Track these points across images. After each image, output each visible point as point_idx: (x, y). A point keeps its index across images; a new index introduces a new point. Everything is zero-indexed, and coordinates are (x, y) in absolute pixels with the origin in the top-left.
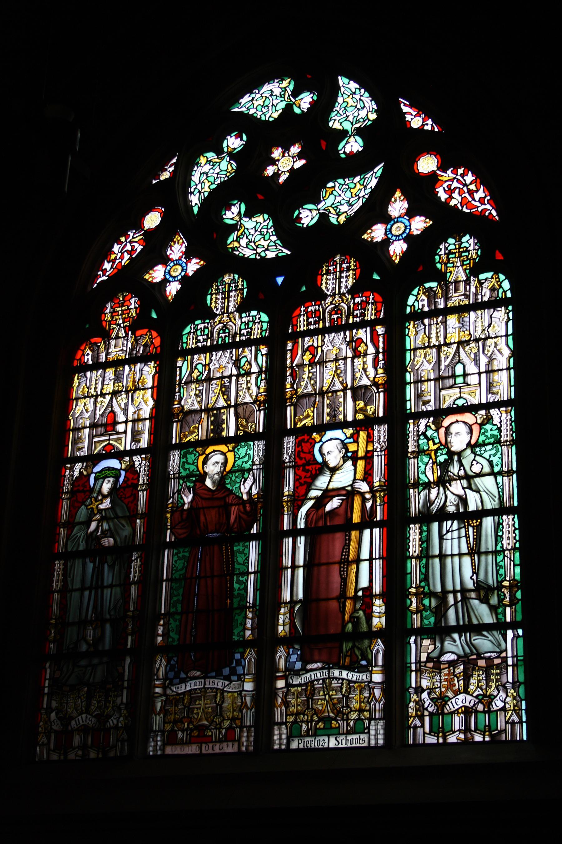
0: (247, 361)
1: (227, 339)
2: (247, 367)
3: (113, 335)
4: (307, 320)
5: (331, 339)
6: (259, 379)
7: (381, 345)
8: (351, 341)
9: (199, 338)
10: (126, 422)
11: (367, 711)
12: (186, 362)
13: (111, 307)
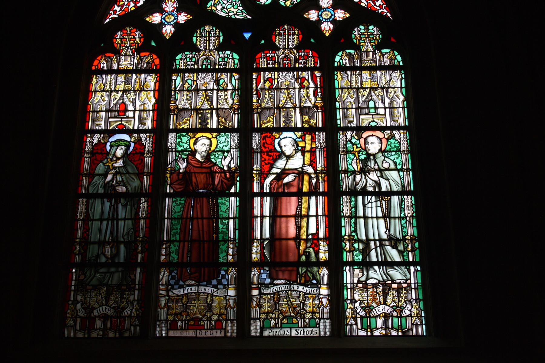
3: (123, 53)
4: (267, 62)
6: (234, 94)
7: (319, 83)
10: (134, 111)
13: (121, 35)
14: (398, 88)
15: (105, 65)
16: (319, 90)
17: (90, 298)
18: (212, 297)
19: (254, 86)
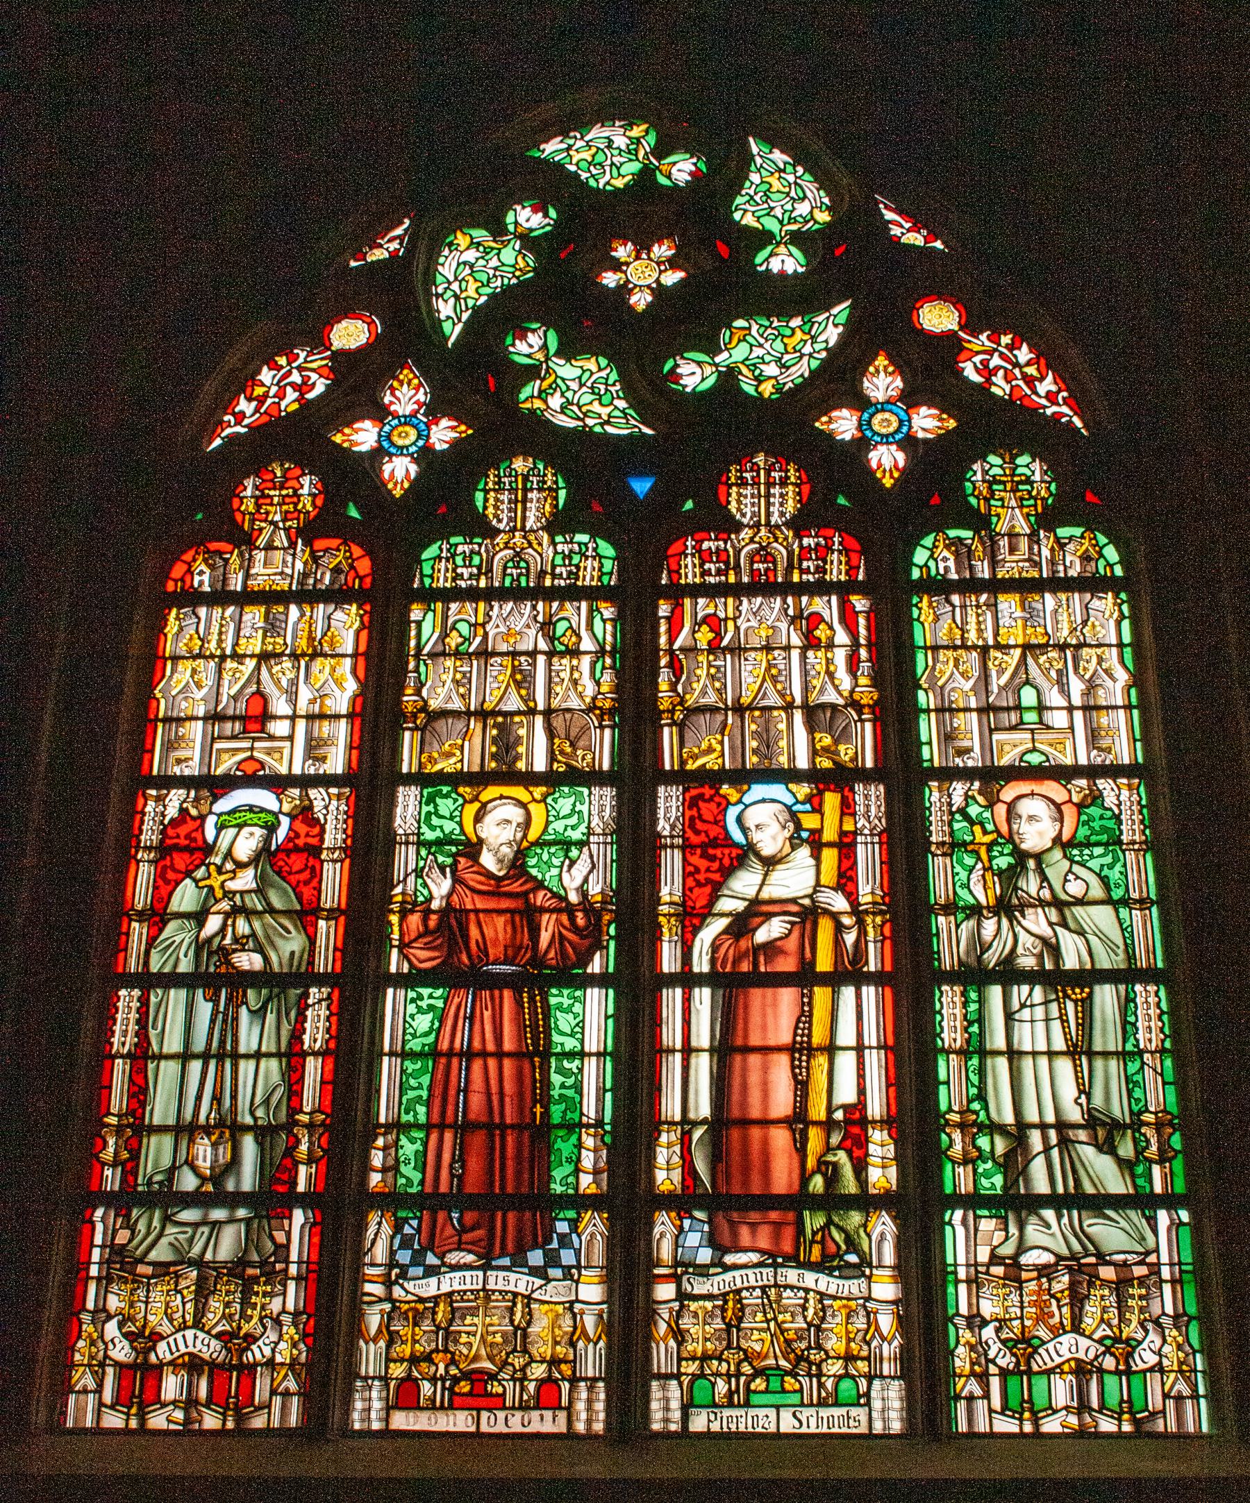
3: (261, 541)
5: (505, 612)
6: (599, 666)
7: (863, 631)
9: (459, 571)
10: (293, 718)
11: (863, 1359)
12: (430, 614)
13: (256, 487)
14: (1110, 646)
15: (206, 578)
16: (863, 653)
17: (147, 1303)
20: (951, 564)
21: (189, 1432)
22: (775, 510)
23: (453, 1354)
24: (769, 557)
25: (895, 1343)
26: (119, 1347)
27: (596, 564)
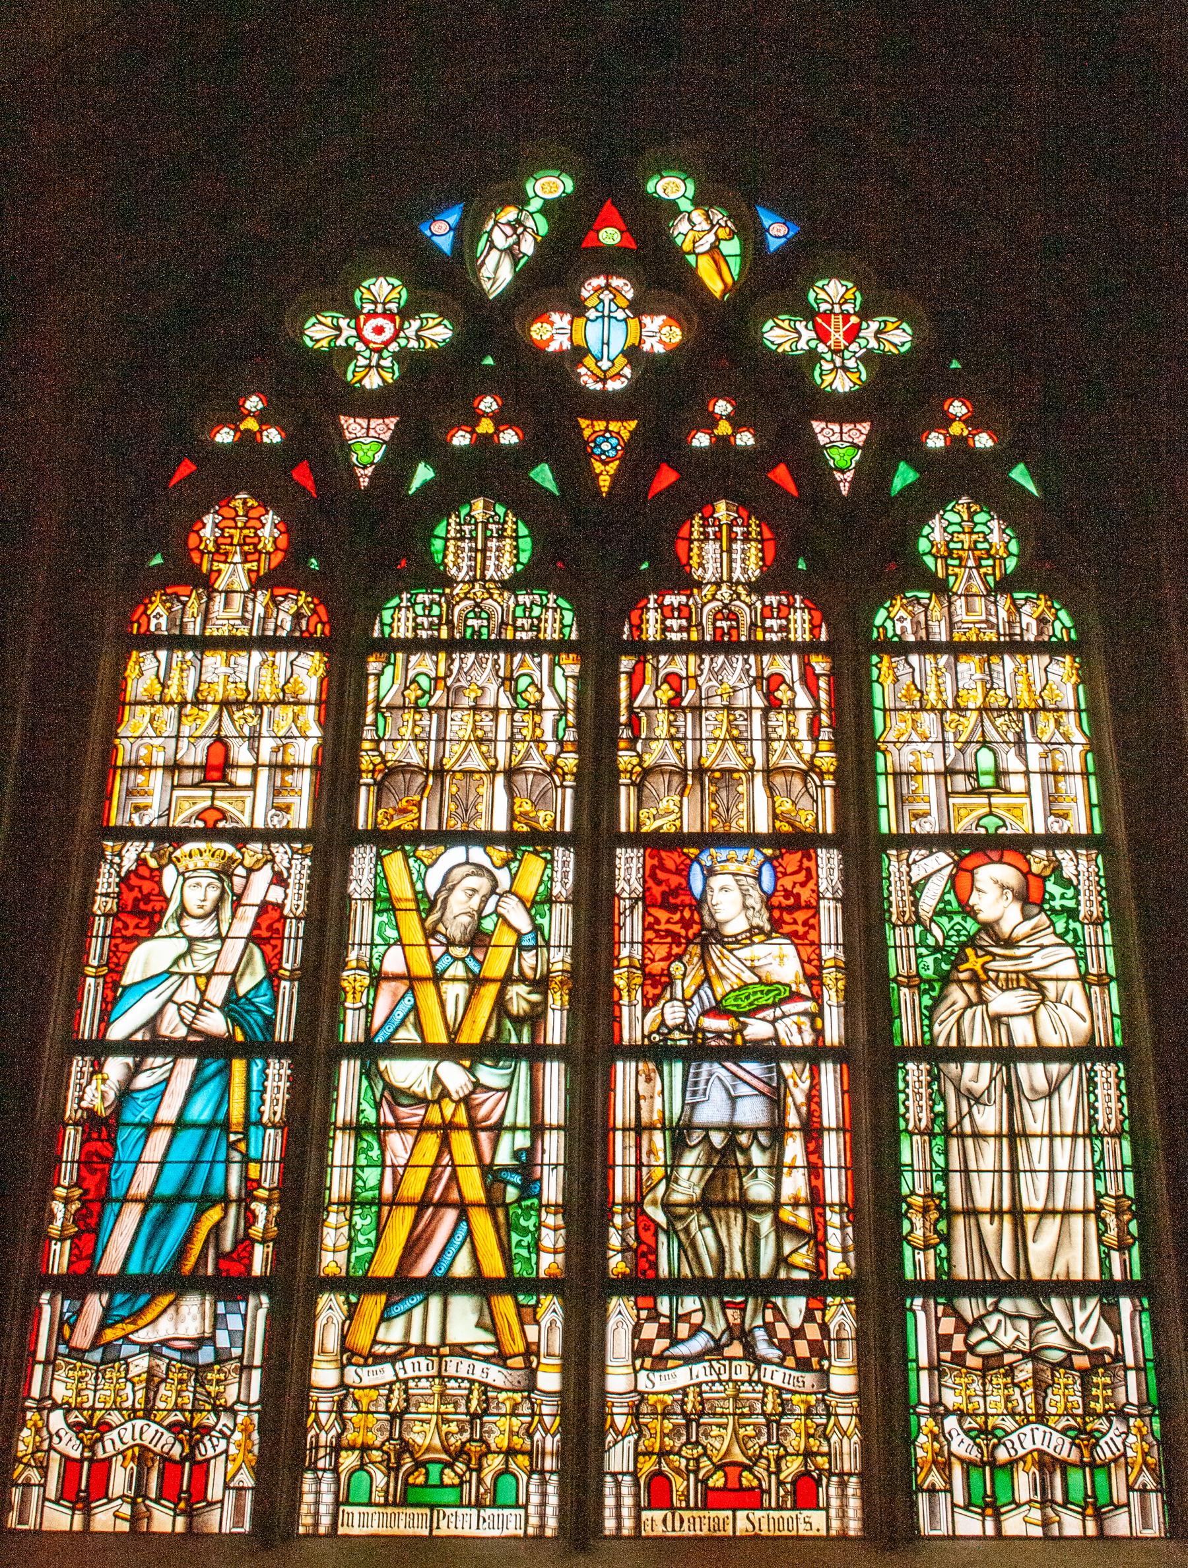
0: (533, 683)
1: (484, 631)
2: (533, 695)
3: (220, 584)
4: (663, 622)
6: (562, 724)
8: (758, 680)
9: (419, 620)
11: (822, 1455)
14: (1067, 711)
15: (163, 621)
16: (825, 719)
18: (485, 1393)
19: (624, 695)
20: (907, 624)
21: (139, 1532)
22: (737, 566)
23: (705, 1448)
24: (733, 616)
25: (855, 1439)
26: (65, 1439)
27: (558, 617)
